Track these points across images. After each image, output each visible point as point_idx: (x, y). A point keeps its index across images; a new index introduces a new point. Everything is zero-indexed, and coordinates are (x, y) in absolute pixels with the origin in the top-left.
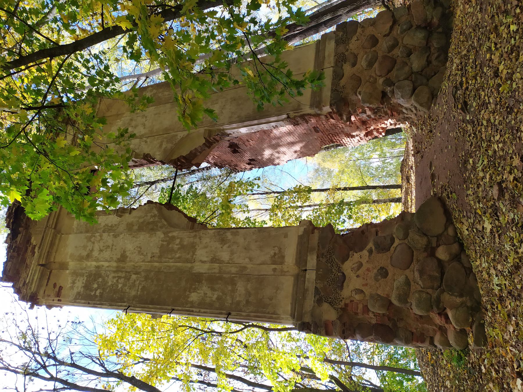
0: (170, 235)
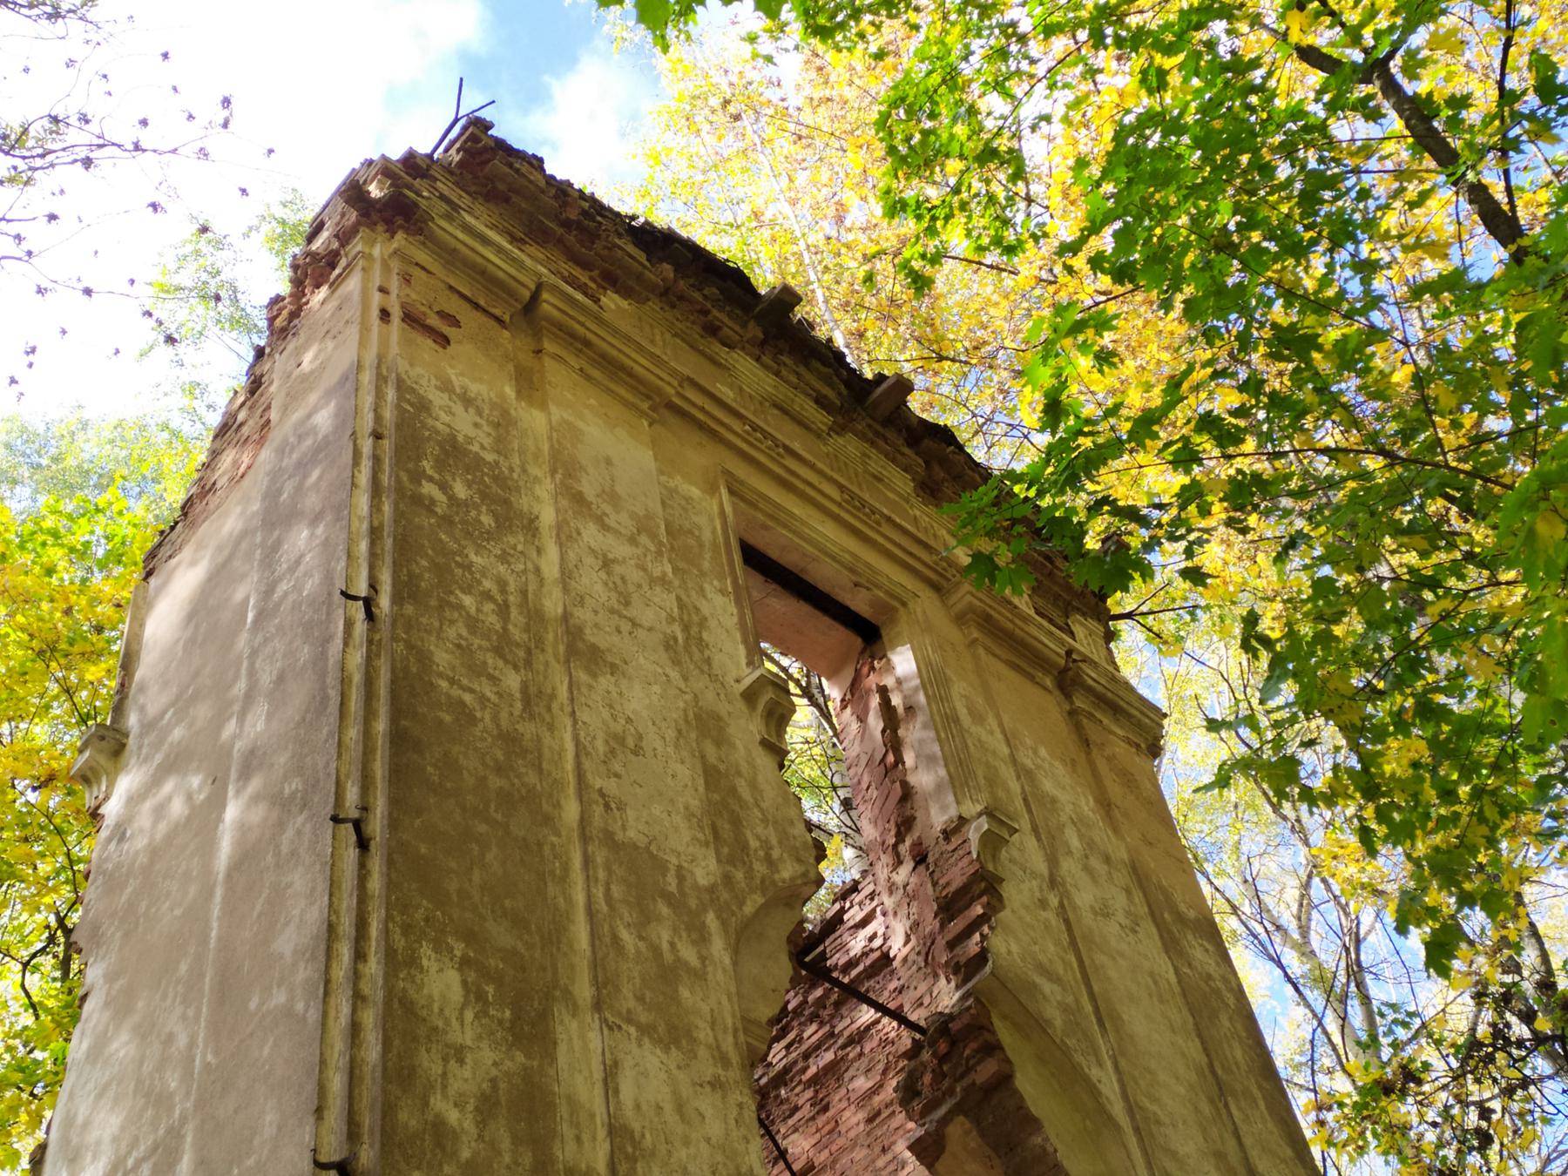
0: (711, 919)
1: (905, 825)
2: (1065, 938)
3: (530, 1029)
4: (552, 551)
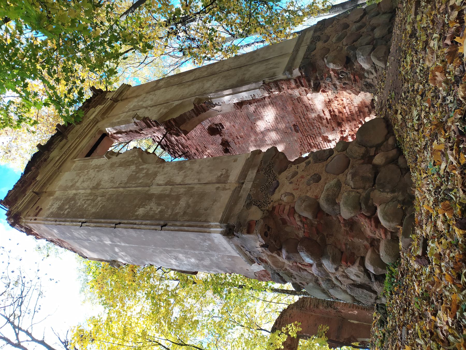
0: (140, 167)
1: (136, 132)
2: (155, 107)
3: (148, 197)
4: (80, 191)
